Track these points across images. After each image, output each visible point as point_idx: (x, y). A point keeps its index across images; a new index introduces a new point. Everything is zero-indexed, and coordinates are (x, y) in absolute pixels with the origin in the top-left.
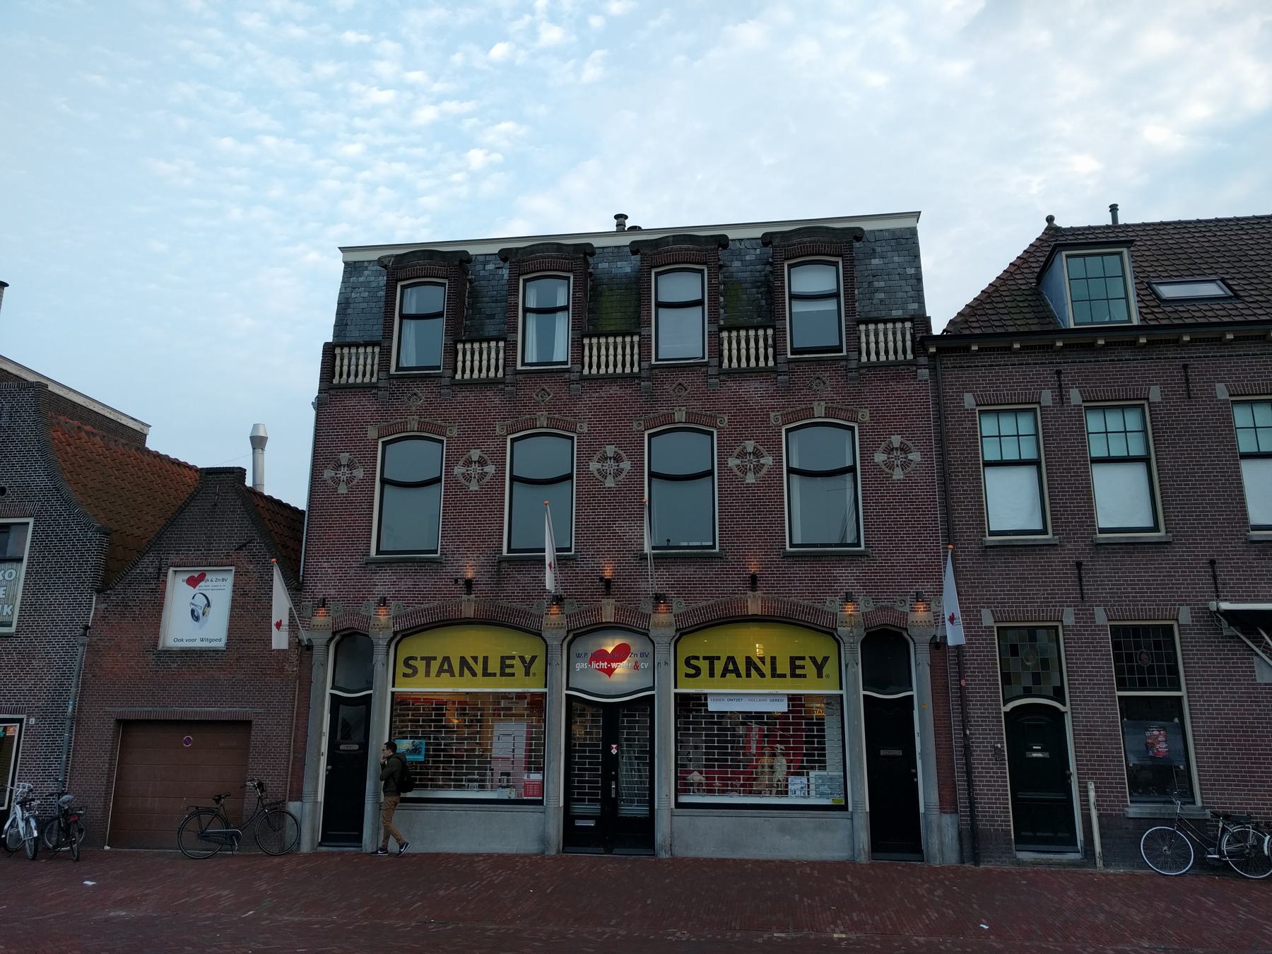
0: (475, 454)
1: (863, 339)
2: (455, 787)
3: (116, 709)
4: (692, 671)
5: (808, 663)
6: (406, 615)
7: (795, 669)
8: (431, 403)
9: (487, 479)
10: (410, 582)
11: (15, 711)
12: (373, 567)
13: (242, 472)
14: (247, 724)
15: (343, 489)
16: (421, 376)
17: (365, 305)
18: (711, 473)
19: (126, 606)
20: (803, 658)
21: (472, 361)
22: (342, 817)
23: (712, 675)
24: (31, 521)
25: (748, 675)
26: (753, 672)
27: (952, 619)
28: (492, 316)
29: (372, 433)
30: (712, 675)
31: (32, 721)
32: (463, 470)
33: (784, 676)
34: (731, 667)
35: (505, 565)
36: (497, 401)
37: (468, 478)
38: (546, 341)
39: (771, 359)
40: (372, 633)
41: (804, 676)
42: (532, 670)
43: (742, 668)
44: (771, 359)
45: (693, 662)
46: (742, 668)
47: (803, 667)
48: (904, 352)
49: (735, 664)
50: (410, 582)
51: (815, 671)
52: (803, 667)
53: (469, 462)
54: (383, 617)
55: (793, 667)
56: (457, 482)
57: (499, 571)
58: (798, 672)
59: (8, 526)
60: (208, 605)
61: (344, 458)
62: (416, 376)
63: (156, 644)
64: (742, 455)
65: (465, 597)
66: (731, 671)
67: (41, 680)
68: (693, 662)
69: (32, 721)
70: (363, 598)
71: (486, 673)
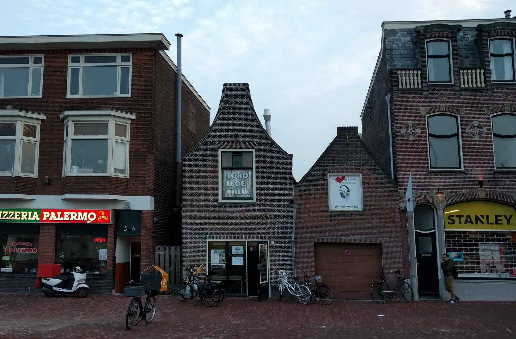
0: (476, 123)
1: (462, 77)
2: (466, 272)
3: (314, 238)
4: (452, 222)
5: (503, 218)
6: (452, 197)
7: (497, 221)
8: (450, 98)
9: (483, 134)
10: (451, 182)
11: (263, 238)
12: (432, 174)
13: (355, 129)
14: (378, 246)
15: (411, 138)
16: (437, 86)
17: (401, 51)
18: (457, 135)
19: (310, 191)
20: (501, 216)
21: (468, 79)
22: (429, 286)
23: (460, 223)
24: (254, 151)
25: (477, 223)
26: (479, 222)
27: (409, 200)
28: (467, 58)
29: (423, 112)
30: (460, 223)
31: (273, 242)
32: (471, 130)
33: (493, 224)
34: (469, 220)
35: (497, 174)
36: (483, 98)
37: (474, 134)
38: (501, 70)
39: (420, 84)
40: (436, 204)
41: (502, 224)
42: (511, 222)
43: (474, 220)
44: (420, 84)
45: (451, 218)
46: (474, 220)
47: (501, 220)
48: (418, 84)
49: (470, 218)
50: (451, 182)
51: (506, 221)
52: (501, 220)
53: (473, 127)
54: (440, 197)
55: (497, 220)
56: (468, 136)
57: (494, 177)
58: (499, 222)
59: (241, 153)
60: (349, 191)
61: (410, 123)
62: (442, 85)
63: (328, 209)
64: (473, 127)
65: (479, 189)
66: (469, 222)
67: (274, 224)
68: (451, 218)
69: (273, 242)
70: (429, 189)
71: (488, 223)
